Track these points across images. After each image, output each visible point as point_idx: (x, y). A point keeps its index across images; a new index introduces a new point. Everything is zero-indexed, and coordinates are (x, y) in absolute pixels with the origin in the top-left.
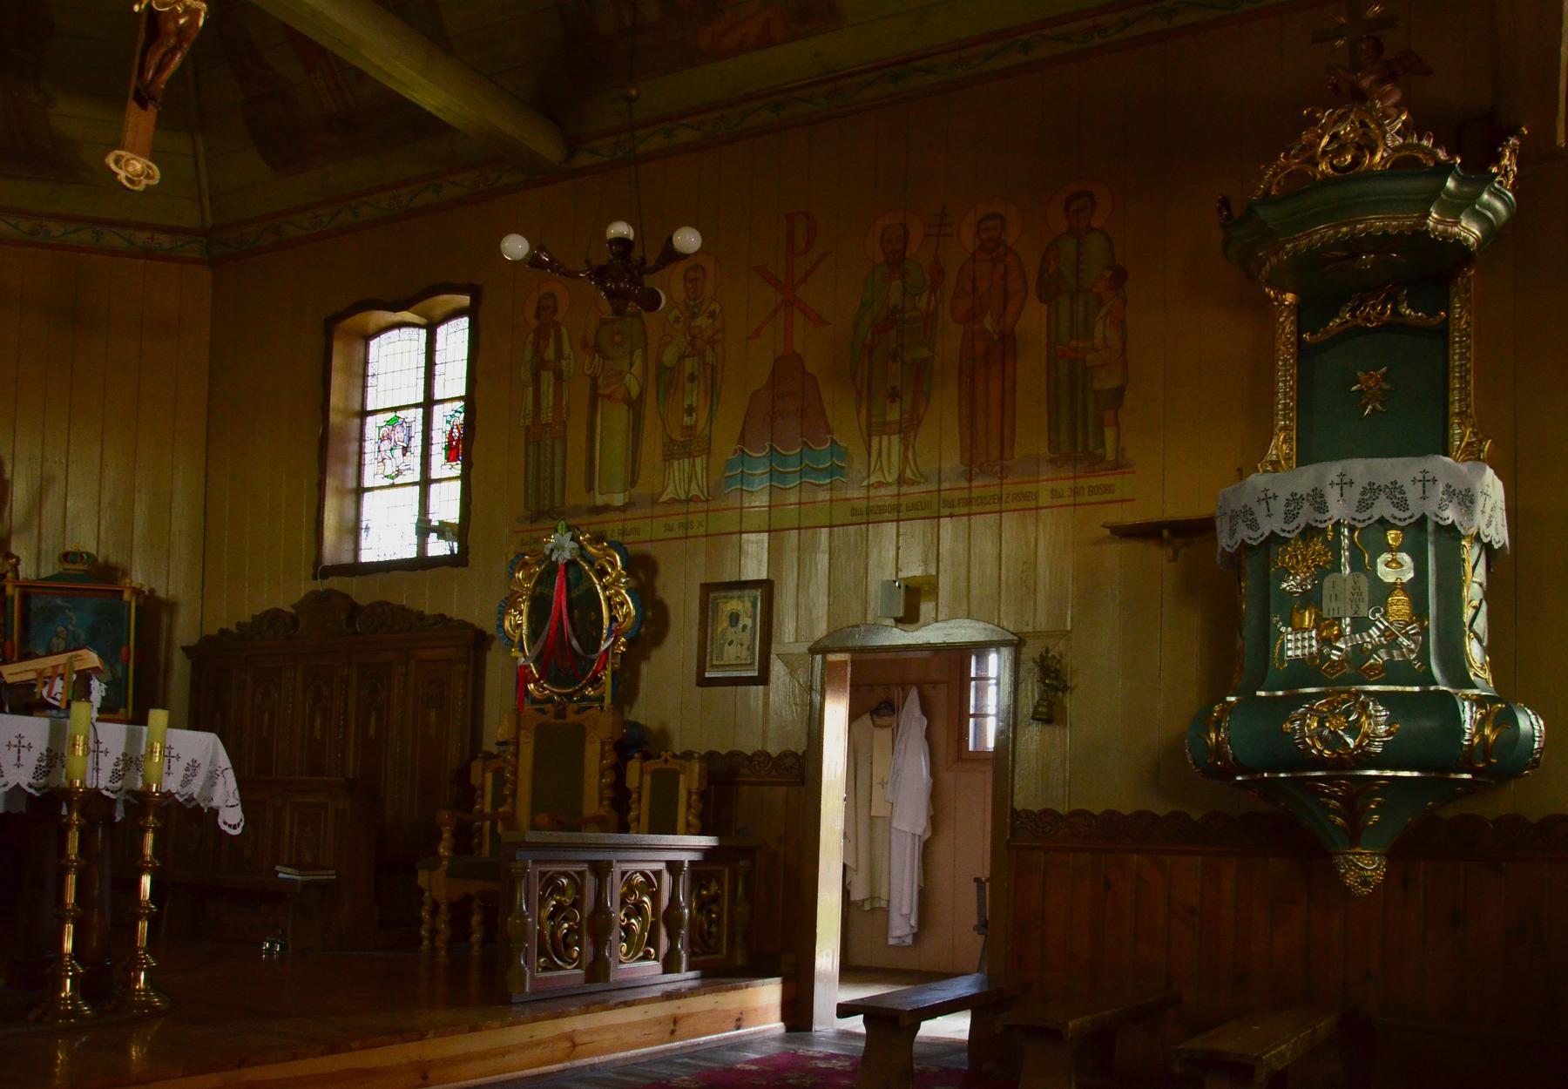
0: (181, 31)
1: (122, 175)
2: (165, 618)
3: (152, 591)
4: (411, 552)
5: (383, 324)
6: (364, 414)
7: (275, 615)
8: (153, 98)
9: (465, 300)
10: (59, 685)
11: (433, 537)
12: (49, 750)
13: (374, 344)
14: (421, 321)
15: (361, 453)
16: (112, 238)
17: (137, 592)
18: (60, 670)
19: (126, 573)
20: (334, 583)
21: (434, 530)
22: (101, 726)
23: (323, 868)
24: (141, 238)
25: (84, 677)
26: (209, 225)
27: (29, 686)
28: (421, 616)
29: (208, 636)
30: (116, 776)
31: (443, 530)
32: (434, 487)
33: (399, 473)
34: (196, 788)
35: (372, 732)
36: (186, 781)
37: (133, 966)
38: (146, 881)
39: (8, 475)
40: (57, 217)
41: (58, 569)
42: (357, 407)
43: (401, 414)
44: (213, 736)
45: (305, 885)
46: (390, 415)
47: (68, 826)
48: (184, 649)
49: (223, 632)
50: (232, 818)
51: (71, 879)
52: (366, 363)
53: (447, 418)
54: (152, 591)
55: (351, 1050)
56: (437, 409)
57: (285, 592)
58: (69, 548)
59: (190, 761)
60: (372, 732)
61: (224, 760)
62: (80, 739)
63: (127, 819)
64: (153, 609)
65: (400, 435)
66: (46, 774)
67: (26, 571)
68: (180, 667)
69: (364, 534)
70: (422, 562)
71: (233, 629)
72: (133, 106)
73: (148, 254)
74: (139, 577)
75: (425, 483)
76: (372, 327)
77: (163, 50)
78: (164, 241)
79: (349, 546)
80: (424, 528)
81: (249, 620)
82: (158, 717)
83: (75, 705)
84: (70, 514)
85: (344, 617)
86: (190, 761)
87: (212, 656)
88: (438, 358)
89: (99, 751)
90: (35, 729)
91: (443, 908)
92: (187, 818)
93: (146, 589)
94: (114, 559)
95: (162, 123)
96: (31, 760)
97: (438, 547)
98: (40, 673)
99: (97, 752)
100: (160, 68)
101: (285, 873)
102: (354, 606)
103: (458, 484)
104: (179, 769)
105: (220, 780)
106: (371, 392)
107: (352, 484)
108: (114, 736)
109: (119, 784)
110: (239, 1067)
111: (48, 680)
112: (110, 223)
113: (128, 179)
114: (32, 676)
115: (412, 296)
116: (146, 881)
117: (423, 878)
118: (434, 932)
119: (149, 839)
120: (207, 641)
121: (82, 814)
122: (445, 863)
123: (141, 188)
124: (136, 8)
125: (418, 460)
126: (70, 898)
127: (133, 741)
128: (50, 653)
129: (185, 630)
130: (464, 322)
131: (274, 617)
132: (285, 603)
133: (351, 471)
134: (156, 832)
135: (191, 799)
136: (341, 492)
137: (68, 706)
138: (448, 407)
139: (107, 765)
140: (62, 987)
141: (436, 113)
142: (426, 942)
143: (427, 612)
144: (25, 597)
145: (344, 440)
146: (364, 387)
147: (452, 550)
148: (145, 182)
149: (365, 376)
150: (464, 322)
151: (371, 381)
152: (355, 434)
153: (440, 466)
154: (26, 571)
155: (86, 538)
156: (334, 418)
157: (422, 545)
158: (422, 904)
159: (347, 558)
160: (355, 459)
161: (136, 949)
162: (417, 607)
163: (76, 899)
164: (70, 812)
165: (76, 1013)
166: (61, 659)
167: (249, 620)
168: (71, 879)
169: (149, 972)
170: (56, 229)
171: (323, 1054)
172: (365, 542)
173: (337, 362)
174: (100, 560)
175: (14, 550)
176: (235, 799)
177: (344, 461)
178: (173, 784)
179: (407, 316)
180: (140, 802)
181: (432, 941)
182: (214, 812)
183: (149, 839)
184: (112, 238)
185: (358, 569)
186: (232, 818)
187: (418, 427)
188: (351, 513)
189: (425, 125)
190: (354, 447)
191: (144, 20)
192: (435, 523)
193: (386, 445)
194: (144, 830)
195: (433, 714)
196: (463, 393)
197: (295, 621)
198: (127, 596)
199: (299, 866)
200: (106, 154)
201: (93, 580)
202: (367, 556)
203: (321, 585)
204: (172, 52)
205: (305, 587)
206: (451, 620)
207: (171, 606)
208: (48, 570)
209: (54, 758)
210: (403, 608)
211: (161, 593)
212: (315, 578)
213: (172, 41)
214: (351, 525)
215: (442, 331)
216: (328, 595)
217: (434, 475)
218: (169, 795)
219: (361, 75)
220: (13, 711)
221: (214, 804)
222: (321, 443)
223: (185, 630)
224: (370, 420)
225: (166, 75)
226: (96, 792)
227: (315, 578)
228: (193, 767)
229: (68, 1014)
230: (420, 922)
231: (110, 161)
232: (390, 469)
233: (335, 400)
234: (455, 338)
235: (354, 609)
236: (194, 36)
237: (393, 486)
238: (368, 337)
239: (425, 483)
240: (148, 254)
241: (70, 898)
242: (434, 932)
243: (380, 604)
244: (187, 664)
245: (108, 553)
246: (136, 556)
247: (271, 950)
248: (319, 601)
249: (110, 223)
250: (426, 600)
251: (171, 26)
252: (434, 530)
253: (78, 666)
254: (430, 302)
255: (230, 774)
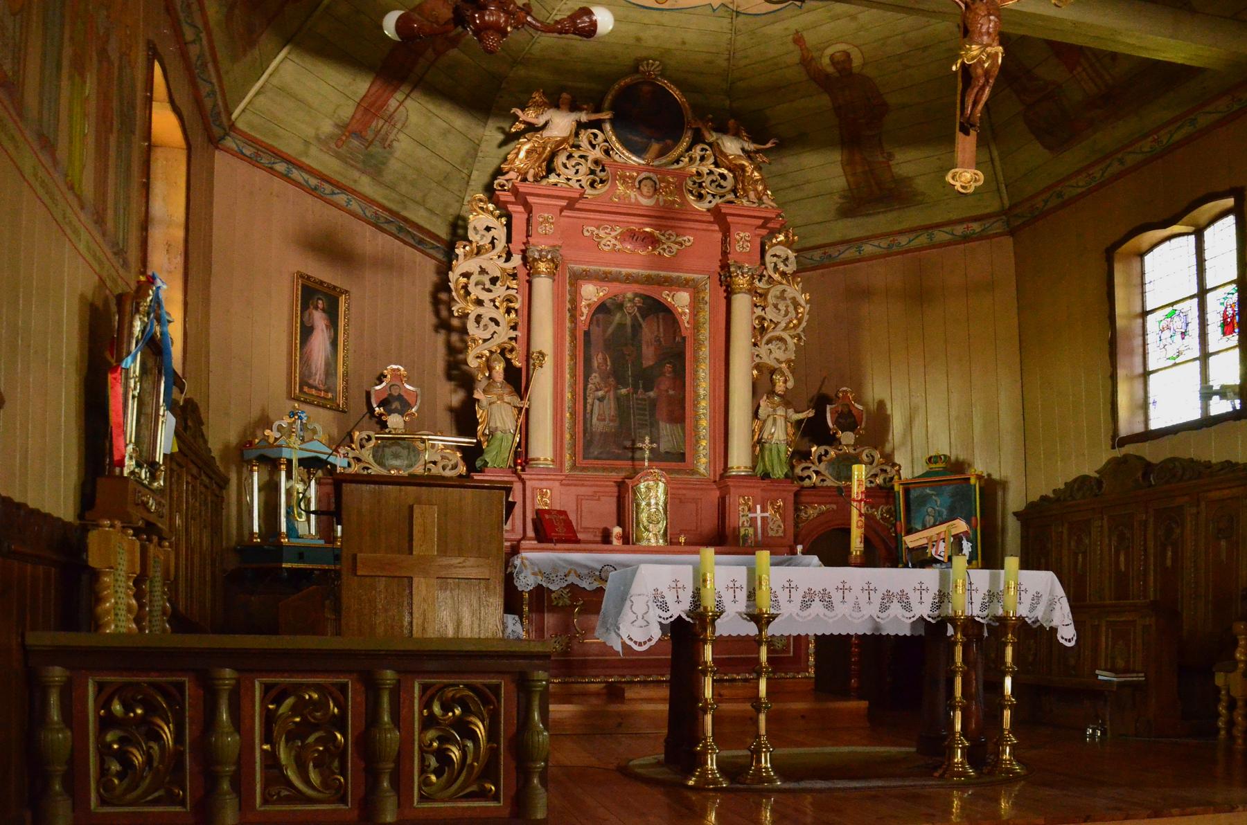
0: (987, 73)
1: (958, 186)
2: (1000, 493)
3: (989, 475)
4: (1195, 414)
5: (1155, 241)
6: (1145, 314)
7: (1083, 480)
8: (972, 126)
9: (1229, 202)
10: (942, 545)
11: (1216, 398)
12: (940, 591)
13: (1148, 258)
14: (1191, 229)
15: (1145, 344)
16: (941, 236)
17: (979, 477)
18: (942, 536)
19: (970, 465)
20: (1129, 449)
21: (1216, 393)
22: (971, 572)
23: (1133, 672)
24: (959, 230)
25: (958, 539)
26: (1007, 203)
27: (923, 548)
28: (1208, 465)
29: (1032, 503)
30: (984, 607)
31: (1223, 393)
32: (1212, 360)
33: (1179, 354)
34: (1039, 613)
35: (1169, 563)
36: (1033, 608)
37: (1001, 741)
38: (1008, 682)
39: (889, 412)
40: (901, 233)
41: (926, 469)
42: (1139, 310)
43: (1175, 307)
44: (1050, 574)
45: (1120, 685)
46: (1169, 309)
47: (955, 643)
48: (1015, 514)
49: (1044, 498)
50: (1067, 634)
51: (958, 681)
52: (1143, 274)
53: (1222, 301)
54: (989, 475)
55: (1172, 816)
56: (1210, 297)
57: (1090, 460)
58: (932, 454)
59: (1037, 595)
60: (1169, 563)
61: (1060, 591)
62: (960, 582)
63: (987, 636)
64: (991, 488)
65: (1178, 324)
66: (939, 607)
67: (906, 474)
68: (1013, 529)
69: (1151, 406)
70: (1207, 422)
71: (1052, 495)
72: (960, 136)
73: (966, 239)
74: (980, 466)
75: (1205, 356)
76: (1145, 246)
77: (975, 90)
78: (976, 227)
79: (1141, 418)
80: (1207, 394)
81: (1062, 487)
82: (1012, 562)
83: (955, 559)
84: (930, 430)
85: (1140, 474)
86: (1037, 595)
87: (1033, 516)
88: (1207, 255)
89: (973, 591)
90: (930, 576)
91: (1240, 703)
92: (1034, 636)
93: (985, 474)
94: (961, 458)
95: (982, 143)
96: (929, 598)
97: (1219, 407)
98: (930, 539)
99: (970, 590)
100: (975, 103)
101: (1103, 676)
102: (1149, 464)
103: (1237, 351)
104: (1027, 599)
105: (1058, 606)
106: (1148, 296)
107: (1140, 370)
108: (981, 577)
109: (985, 613)
110: (1085, 821)
111: (935, 544)
112: (938, 226)
113: (963, 187)
114: (925, 541)
115: (1176, 210)
116: (1008, 682)
117: (1220, 679)
118: (1231, 723)
119: (1009, 651)
120: (1031, 506)
121: (964, 635)
122: (1241, 665)
123: (971, 190)
124: (954, 68)
125: (1197, 340)
126: (958, 692)
127: (994, 581)
128: (925, 528)
129: (1015, 501)
130: (1230, 220)
131: (1082, 481)
132: (1090, 468)
133: (1138, 360)
134: (1013, 644)
135: (1037, 621)
136: (1131, 378)
137: (950, 559)
138: (1220, 293)
139: (978, 599)
140: (953, 755)
141: (1188, 63)
142: (1223, 732)
143: (1214, 461)
144: (907, 491)
145: (1129, 338)
146: (1143, 293)
147: (1234, 408)
148: (973, 185)
149: (1143, 284)
150: (1230, 220)
151: (1148, 288)
152: (1139, 331)
153: (1216, 339)
154: (906, 474)
155: (942, 446)
156: (1120, 323)
157: (1205, 407)
158: (1219, 700)
159: (1139, 428)
160: (1141, 350)
161: (1002, 730)
162: (1204, 458)
163: (962, 694)
164: (956, 633)
165: (964, 774)
166: (943, 528)
167: (1062, 487)
168: (958, 681)
169: (1013, 747)
170: (903, 240)
171: (1149, 817)
172: (1153, 412)
173: (1119, 279)
174: (953, 458)
175: (897, 460)
176: (1069, 619)
177: (1131, 353)
178: (1023, 611)
179: (1176, 229)
180: (1001, 624)
181: (1229, 732)
182: (1054, 630)
183: (1009, 651)
184: (941, 236)
185: (1148, 436)
186: (1067, 634)
187: (1194, 314)
188: (1141, 393)
189: (1169, 76)
190: (1139, 341)
191: (960, 74)
192: (1216, 387)
193: (1167, 334)
194: (1005, 645)
195: (1223, 543)
196: (1235, 276)
197: (1099, 482)
198: (973, 481)
199: (1113, 670)
200: (944, 177)
201: (950, 473)
202: (1154, 425)
203: (1119, 453)
204: (982, 88)
205: (1105, 455)
206: (1237, 464)
207: (1003, 484)
208: (919, 471)
209: (943, 597)
210: (1191, 460)
211: (996, 476)
212: (1113, 447)
213: (982, 81)
214: (1141, 401)
215: (1208, 234)
216: (1125, 459)
217: (1211, 349)
218: (1021, 619)
219: (1114, 56)
220: (914, 566)
221: (1054, 624)
222: (1109, 342)
223: (1015, 501)
224: (1149, 317)
225: (980, 107)
226: (971, 619)
227: (1113, 447)
228: (1037, 597)
229: (959, 775)
230: (1218, 715)
231: (949, 178)
232: (1172, 351)
233: (1120, 309)
234: (1223, 237)
235: (1148, 467)
236: (996, 71)
237: (1175, 365)
238: (1142, 255)
239: (1205, 356)
240: (966, 239)
241: (958, 692)
242: (1231, 723)
243: (1173, 460)
244: (1018, 524)
245: (957, 453)
246: (977, 452)
247: (1093, 735)
248: (1117, 466)
249: (938, 226)
250: (1213, 451)
251: (980, 71)
252: (1216, 393)
253: (954, 532)
254: (1195, 213)
255: (1065, 601)
